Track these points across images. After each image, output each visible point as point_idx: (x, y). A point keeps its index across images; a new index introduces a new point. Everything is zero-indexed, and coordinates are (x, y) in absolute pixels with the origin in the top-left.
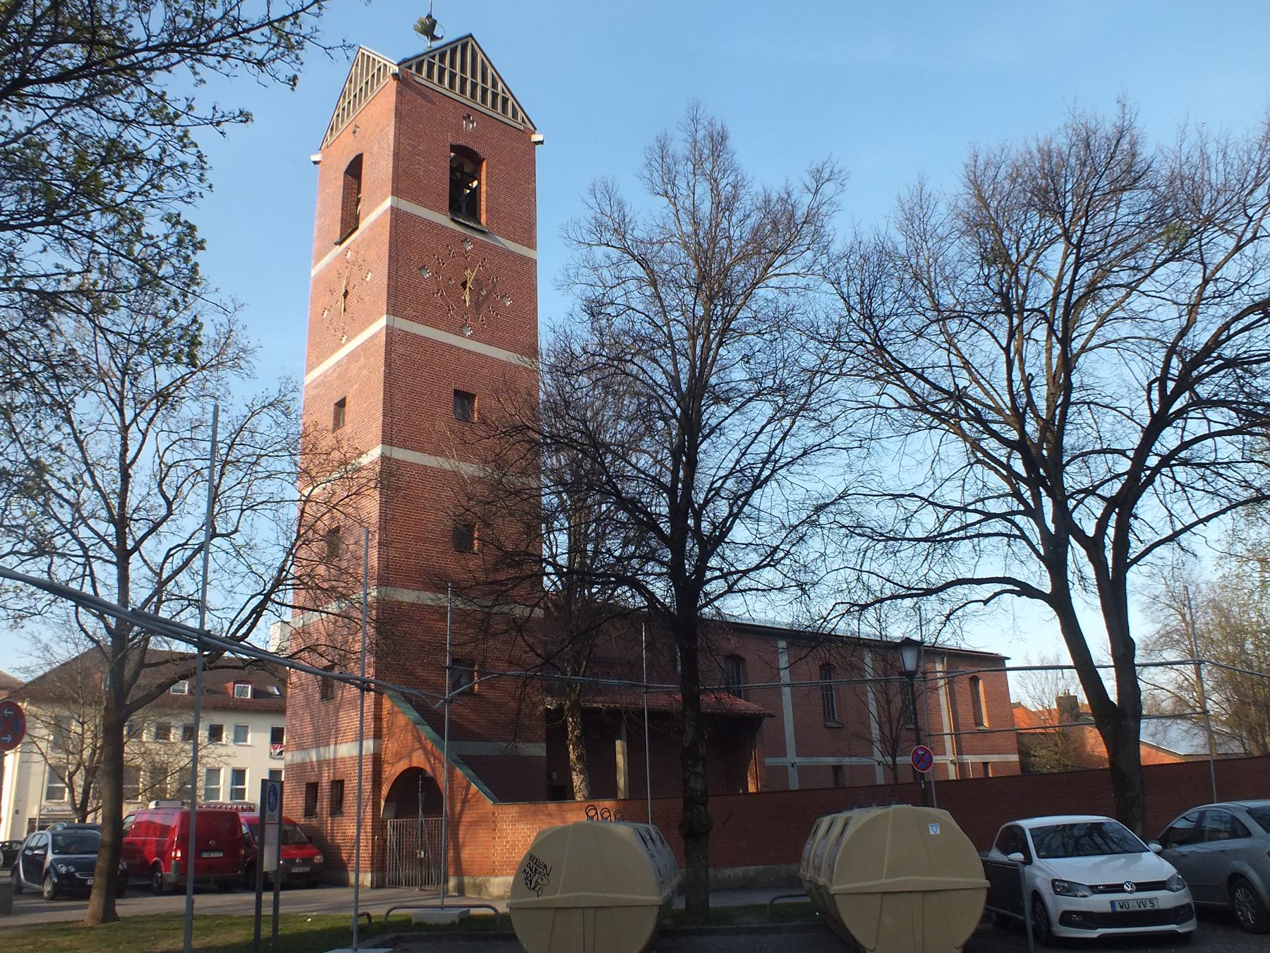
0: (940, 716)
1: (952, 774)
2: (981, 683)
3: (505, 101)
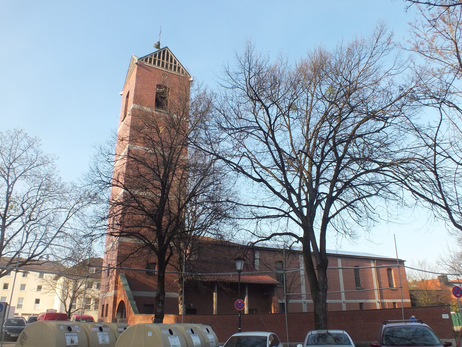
0: (373, 284)
1: (378, 307)
2: (392, 270)
3: (179, 68)
